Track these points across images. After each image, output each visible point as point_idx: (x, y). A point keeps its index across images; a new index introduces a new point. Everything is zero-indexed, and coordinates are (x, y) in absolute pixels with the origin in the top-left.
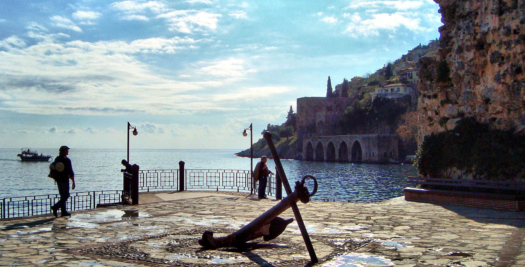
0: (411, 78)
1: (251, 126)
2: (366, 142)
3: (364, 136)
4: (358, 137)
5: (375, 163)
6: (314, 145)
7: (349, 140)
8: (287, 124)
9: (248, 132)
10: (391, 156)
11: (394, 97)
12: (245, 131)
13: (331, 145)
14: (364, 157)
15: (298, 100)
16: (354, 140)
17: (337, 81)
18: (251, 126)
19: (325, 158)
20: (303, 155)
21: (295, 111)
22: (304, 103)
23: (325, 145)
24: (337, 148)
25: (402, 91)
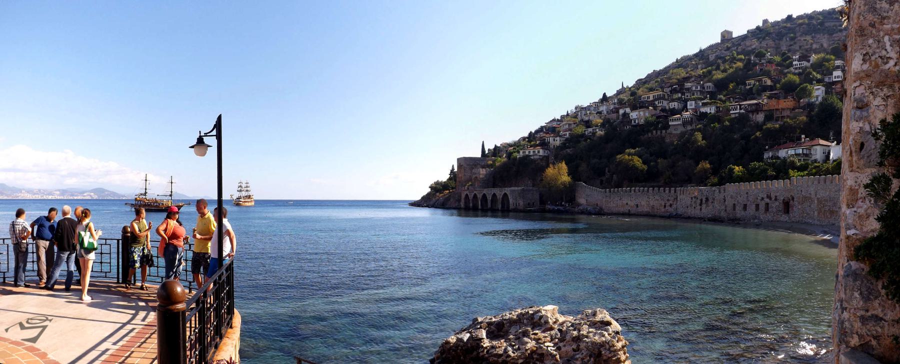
1: (218, 126)
2: (512, 193)
3: (513, 188)
4: (507, 190)
5: (521, 211)
6: (471, 196)
7: (499, 192)
8: (450, 179)
9: (211, 141)
11: (536, 157)
12: (200, 141)
13: (484, 196)
14: (511, 207)
15: (458, 159)
17: (489, 146)
18: (218, 126)
20: (462, 205)
21: (456, 170)
22: (465, 163)
23: (480, 196)
24: (489, 198)
25: (542, 152)
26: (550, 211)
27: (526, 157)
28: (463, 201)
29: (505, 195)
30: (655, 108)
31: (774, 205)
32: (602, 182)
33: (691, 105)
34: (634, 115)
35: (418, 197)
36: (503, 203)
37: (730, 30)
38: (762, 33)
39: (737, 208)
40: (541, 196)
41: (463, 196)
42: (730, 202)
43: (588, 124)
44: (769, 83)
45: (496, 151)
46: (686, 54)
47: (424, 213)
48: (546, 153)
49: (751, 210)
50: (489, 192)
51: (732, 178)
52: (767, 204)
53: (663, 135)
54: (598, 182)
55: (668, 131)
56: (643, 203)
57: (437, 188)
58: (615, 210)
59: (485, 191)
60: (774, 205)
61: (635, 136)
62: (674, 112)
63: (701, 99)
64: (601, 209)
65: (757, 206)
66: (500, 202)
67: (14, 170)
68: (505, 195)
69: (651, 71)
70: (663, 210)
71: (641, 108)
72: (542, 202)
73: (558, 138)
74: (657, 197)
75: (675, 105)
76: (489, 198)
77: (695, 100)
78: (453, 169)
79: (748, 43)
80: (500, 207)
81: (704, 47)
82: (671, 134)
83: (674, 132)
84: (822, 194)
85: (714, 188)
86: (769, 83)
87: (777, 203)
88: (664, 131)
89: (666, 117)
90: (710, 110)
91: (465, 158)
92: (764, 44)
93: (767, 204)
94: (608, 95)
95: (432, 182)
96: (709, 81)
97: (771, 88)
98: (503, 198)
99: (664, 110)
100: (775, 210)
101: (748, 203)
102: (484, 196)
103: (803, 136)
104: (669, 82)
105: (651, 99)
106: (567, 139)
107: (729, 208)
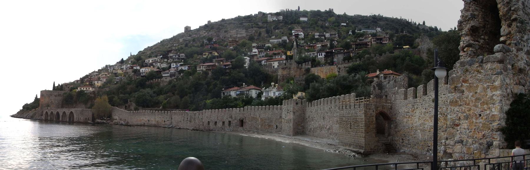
2: (77, 111)
4: (73, 110)
7: (67, 111)
14: (75, 120)
20: (43, 117)
23: (55, 113)
26: (98, 123)
27: (82, 91)
29: (72, 112)
31: (234, 122)
32: (126, 106)
33: (173, 65)
34: (143, 70)
36: (70, 118)
38: (209, 26)
39: (211, 124)
40: (93, 115)
41: (44, 113)
42: (205, 120)
43: (116, 75)
44: (216, 54)
48: (93, 89)
49: (220, 124)
50: (61, 111)
51: (206, 107)
52: (230, 122)
54: (124, 107)
55: (162, 79)
56: (152, 119)
57: (27, 108)
58: (135, 123)
59: (59, 110)
60: (234, 122)
61: (144, 82)
62: (164, 69)
64: (128, 122)
65: (224, 123)
66: (68, 116)
68: (72, 112)
69: (146, 47)
70: (163, 123)
71: (146, 66)
72: (94, 119)
73: (100, 82)
74: (160, 116)
75: (164, 65)
77: (175, 62)
79: (201, 33)
80: (68, 120)
81: (175, 35)
82: (163, 81)
84: (263, 116)
85: (195, 112)
86: (216, 54)
87: (236, 121)
89: (160, 72)
90: (185, 68)
91: (46, 91)
92: (210, 33)
93: (230, 122)
94: (125, 59)
96: (183, 53)
97: (217, 57)
98: (70, 115)
100: (234, 125)
101: (218, 121)
103: (244, 84)
104: (164, 50)
105: (151, 62)
106: (105, 82)
107: (206, 124)
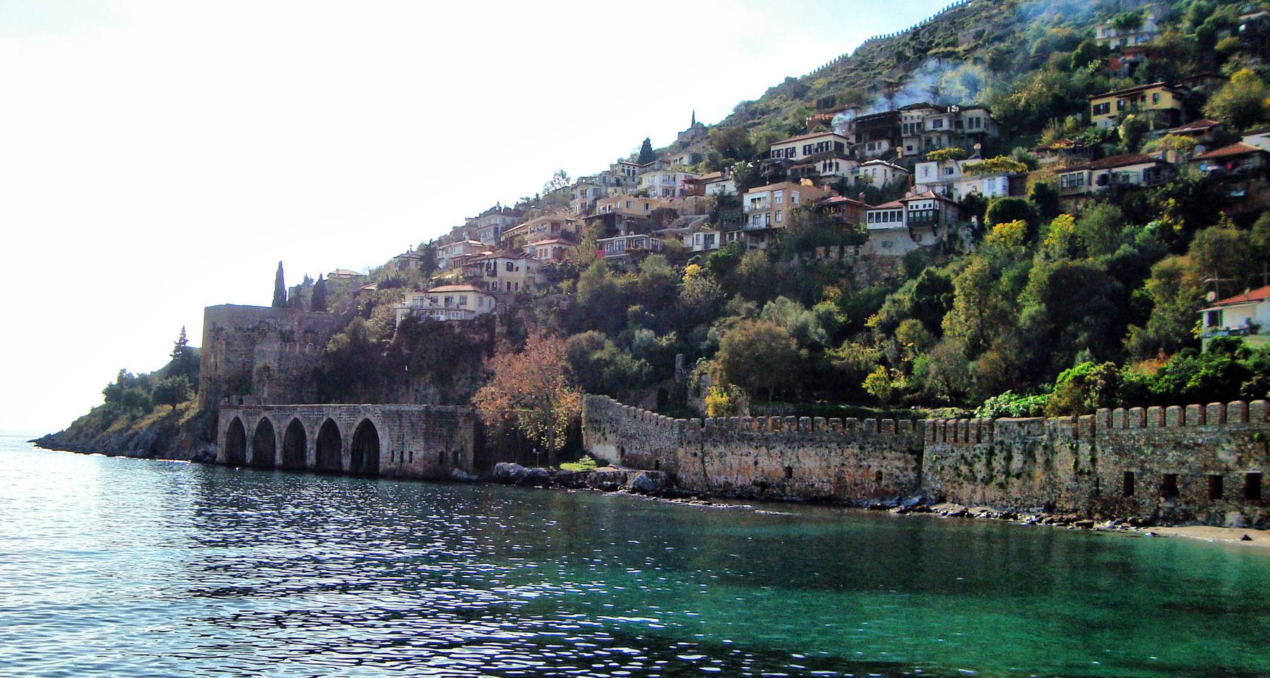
0: (494, 274)
4: (373, 412)
7: (346, 417)
10: (456, 463)
13: (296, 427)
14: (384, 463)
15: (209, 311)
16: (360, 420)
17: (292, 281)
19: (279, 460)
20: (220, 452)
23: (280, 427)
24: (312, 435)
28: (222, 439)
30: (817, 180)
32: (662, 394)
35: (60, 423)
37: (106, 386)
41: (224, 425)
45: (320, 292)
46: (402, 250)
47: (89, 468)
53: (848, 260)
54: (653, 395)
55: (864, 250)
59: (300, 412)
63: (958, 157)
67: (532, 481)
69: (777, 80)
76: (312, 435)
78: (183, 340)
83: (881, 252)
88: (850, 250)
94: (655, 146)
95: (736, 103)
99: (841, 187)
102: (296, 427)
